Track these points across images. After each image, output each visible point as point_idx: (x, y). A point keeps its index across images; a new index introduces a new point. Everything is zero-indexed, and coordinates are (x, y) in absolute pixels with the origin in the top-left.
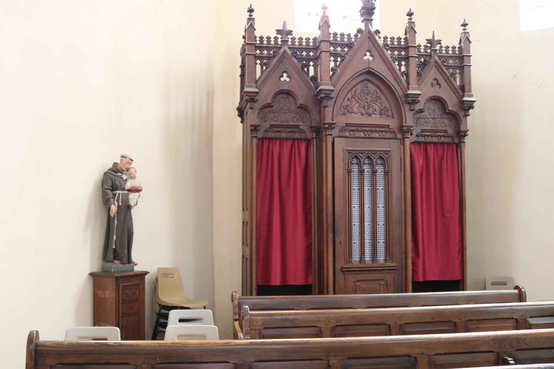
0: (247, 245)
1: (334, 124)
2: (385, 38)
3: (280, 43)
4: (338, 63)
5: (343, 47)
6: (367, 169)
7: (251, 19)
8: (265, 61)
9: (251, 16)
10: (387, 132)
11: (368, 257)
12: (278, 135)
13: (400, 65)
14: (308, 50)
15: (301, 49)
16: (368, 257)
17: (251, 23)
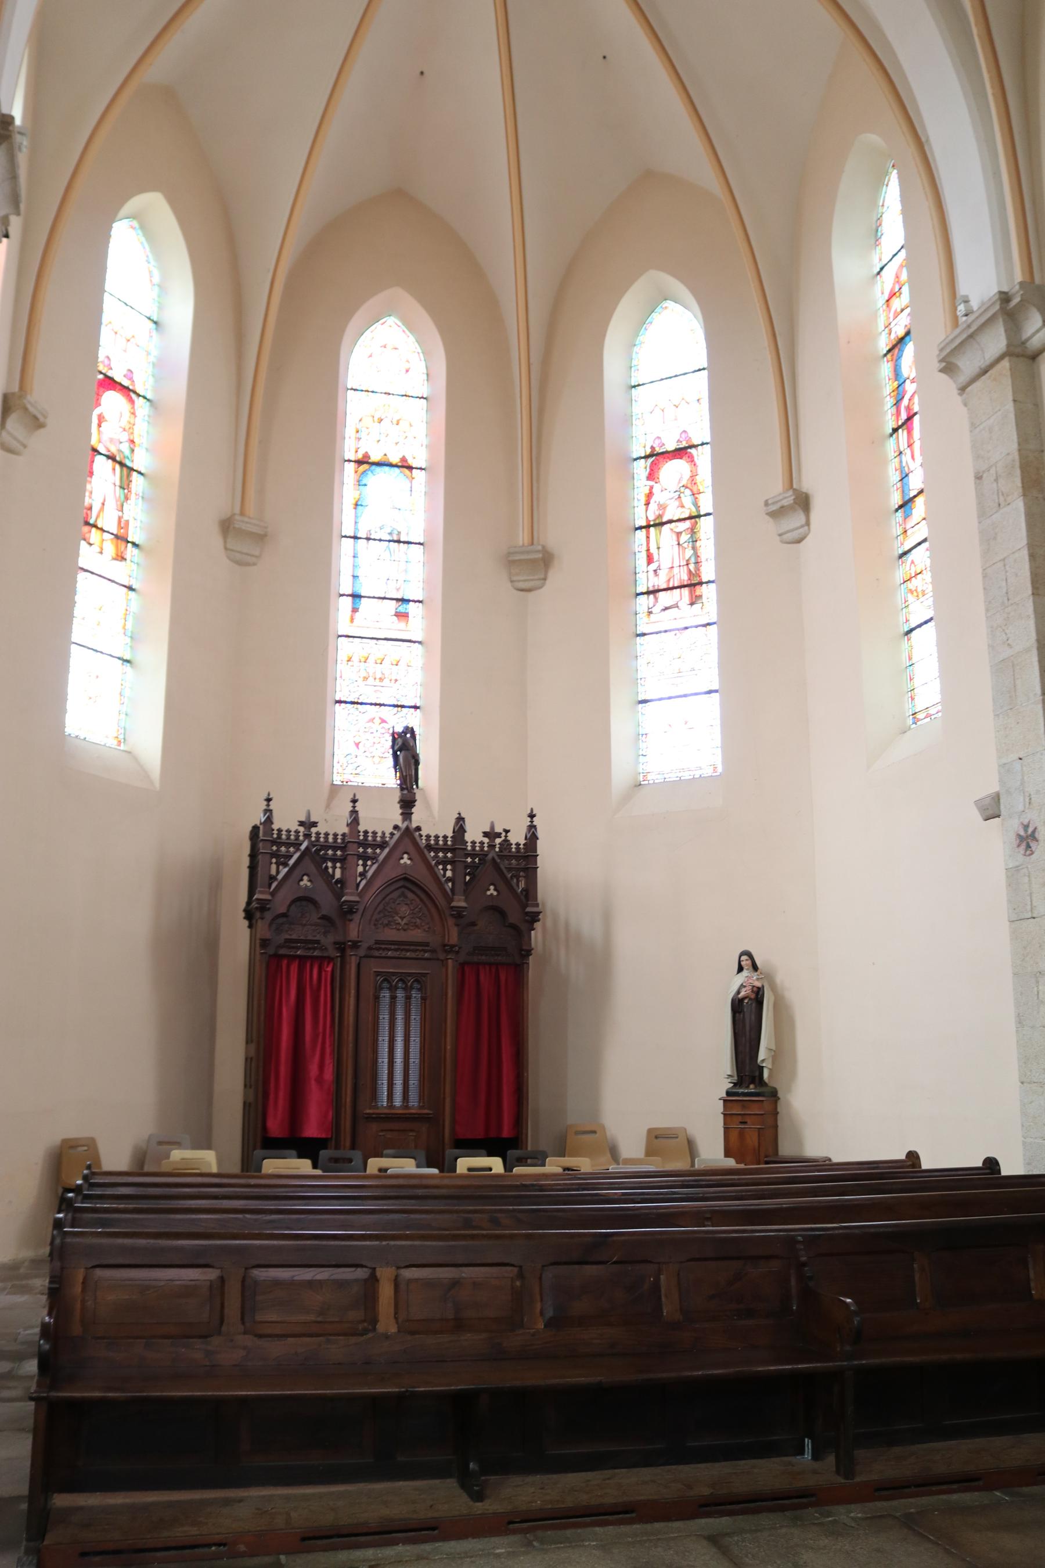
0: (251, 1087)
1: (360, 942)
2: (428, 837)
3: (486, 849)
4: (367, 868)
5: (445, 852)
6: (400, 994)
7: (354, 812)
8: (282, 859)
9: (354, 807)
10: (425, 951)
11: (398, 1101)
12: (309, 953)
13: (445, 870)
14: (335, 848)
15: (326, 847)
16: (398, 1101)
17: (461, 824)
